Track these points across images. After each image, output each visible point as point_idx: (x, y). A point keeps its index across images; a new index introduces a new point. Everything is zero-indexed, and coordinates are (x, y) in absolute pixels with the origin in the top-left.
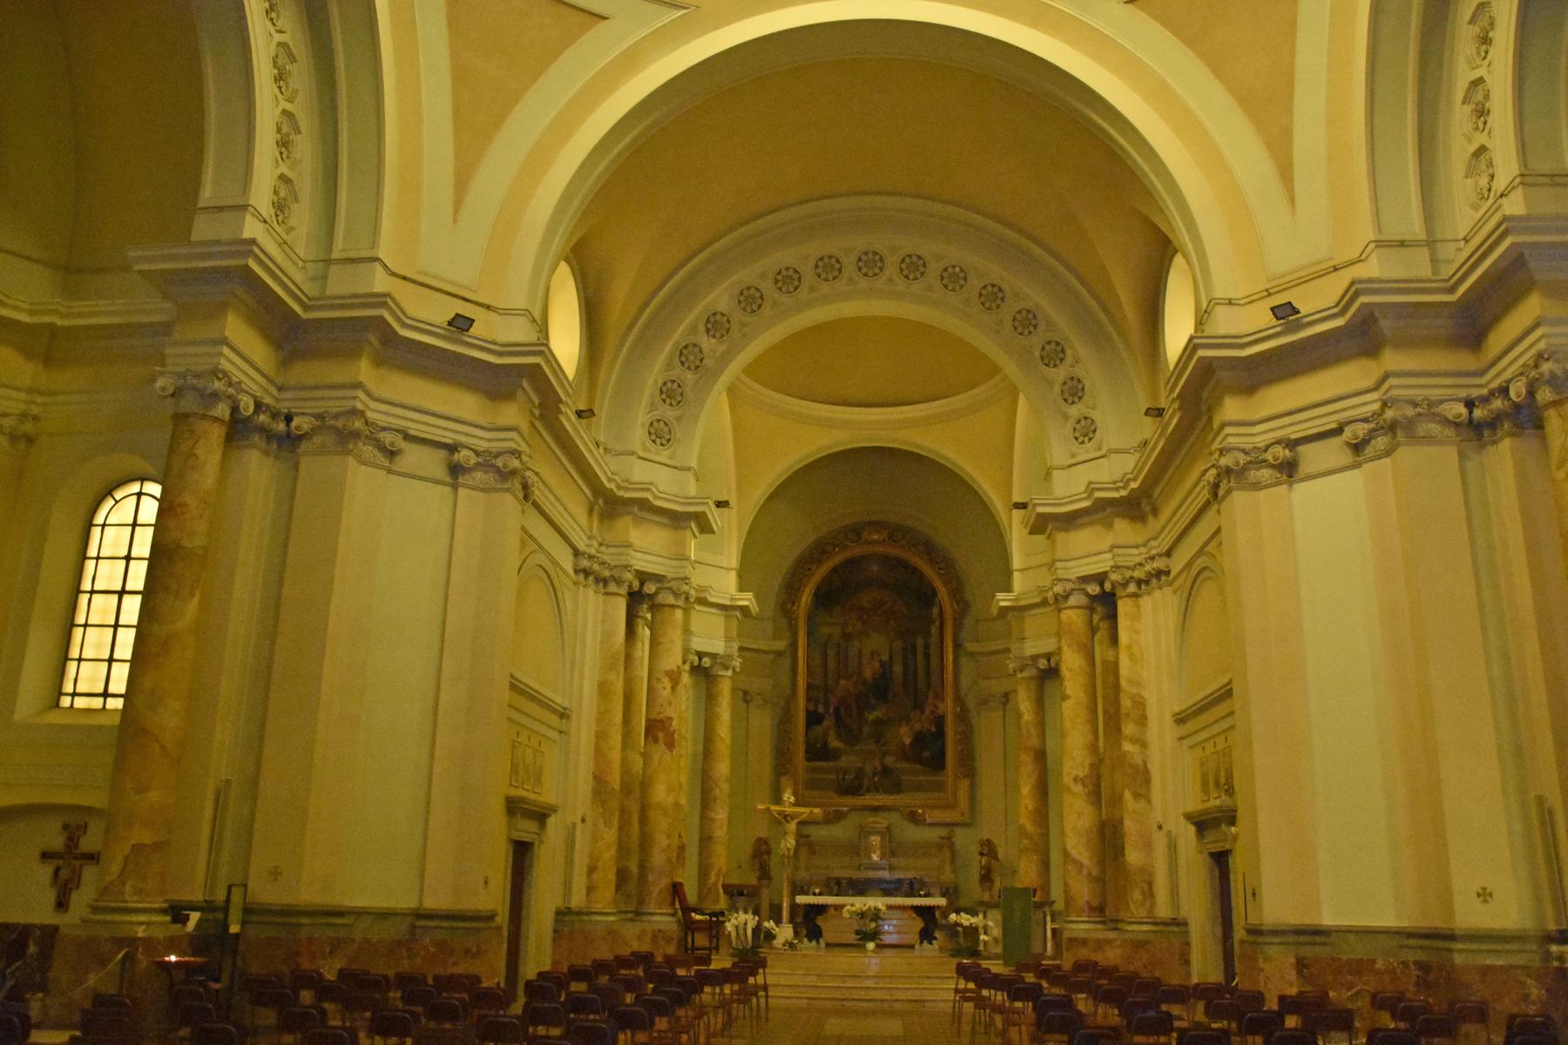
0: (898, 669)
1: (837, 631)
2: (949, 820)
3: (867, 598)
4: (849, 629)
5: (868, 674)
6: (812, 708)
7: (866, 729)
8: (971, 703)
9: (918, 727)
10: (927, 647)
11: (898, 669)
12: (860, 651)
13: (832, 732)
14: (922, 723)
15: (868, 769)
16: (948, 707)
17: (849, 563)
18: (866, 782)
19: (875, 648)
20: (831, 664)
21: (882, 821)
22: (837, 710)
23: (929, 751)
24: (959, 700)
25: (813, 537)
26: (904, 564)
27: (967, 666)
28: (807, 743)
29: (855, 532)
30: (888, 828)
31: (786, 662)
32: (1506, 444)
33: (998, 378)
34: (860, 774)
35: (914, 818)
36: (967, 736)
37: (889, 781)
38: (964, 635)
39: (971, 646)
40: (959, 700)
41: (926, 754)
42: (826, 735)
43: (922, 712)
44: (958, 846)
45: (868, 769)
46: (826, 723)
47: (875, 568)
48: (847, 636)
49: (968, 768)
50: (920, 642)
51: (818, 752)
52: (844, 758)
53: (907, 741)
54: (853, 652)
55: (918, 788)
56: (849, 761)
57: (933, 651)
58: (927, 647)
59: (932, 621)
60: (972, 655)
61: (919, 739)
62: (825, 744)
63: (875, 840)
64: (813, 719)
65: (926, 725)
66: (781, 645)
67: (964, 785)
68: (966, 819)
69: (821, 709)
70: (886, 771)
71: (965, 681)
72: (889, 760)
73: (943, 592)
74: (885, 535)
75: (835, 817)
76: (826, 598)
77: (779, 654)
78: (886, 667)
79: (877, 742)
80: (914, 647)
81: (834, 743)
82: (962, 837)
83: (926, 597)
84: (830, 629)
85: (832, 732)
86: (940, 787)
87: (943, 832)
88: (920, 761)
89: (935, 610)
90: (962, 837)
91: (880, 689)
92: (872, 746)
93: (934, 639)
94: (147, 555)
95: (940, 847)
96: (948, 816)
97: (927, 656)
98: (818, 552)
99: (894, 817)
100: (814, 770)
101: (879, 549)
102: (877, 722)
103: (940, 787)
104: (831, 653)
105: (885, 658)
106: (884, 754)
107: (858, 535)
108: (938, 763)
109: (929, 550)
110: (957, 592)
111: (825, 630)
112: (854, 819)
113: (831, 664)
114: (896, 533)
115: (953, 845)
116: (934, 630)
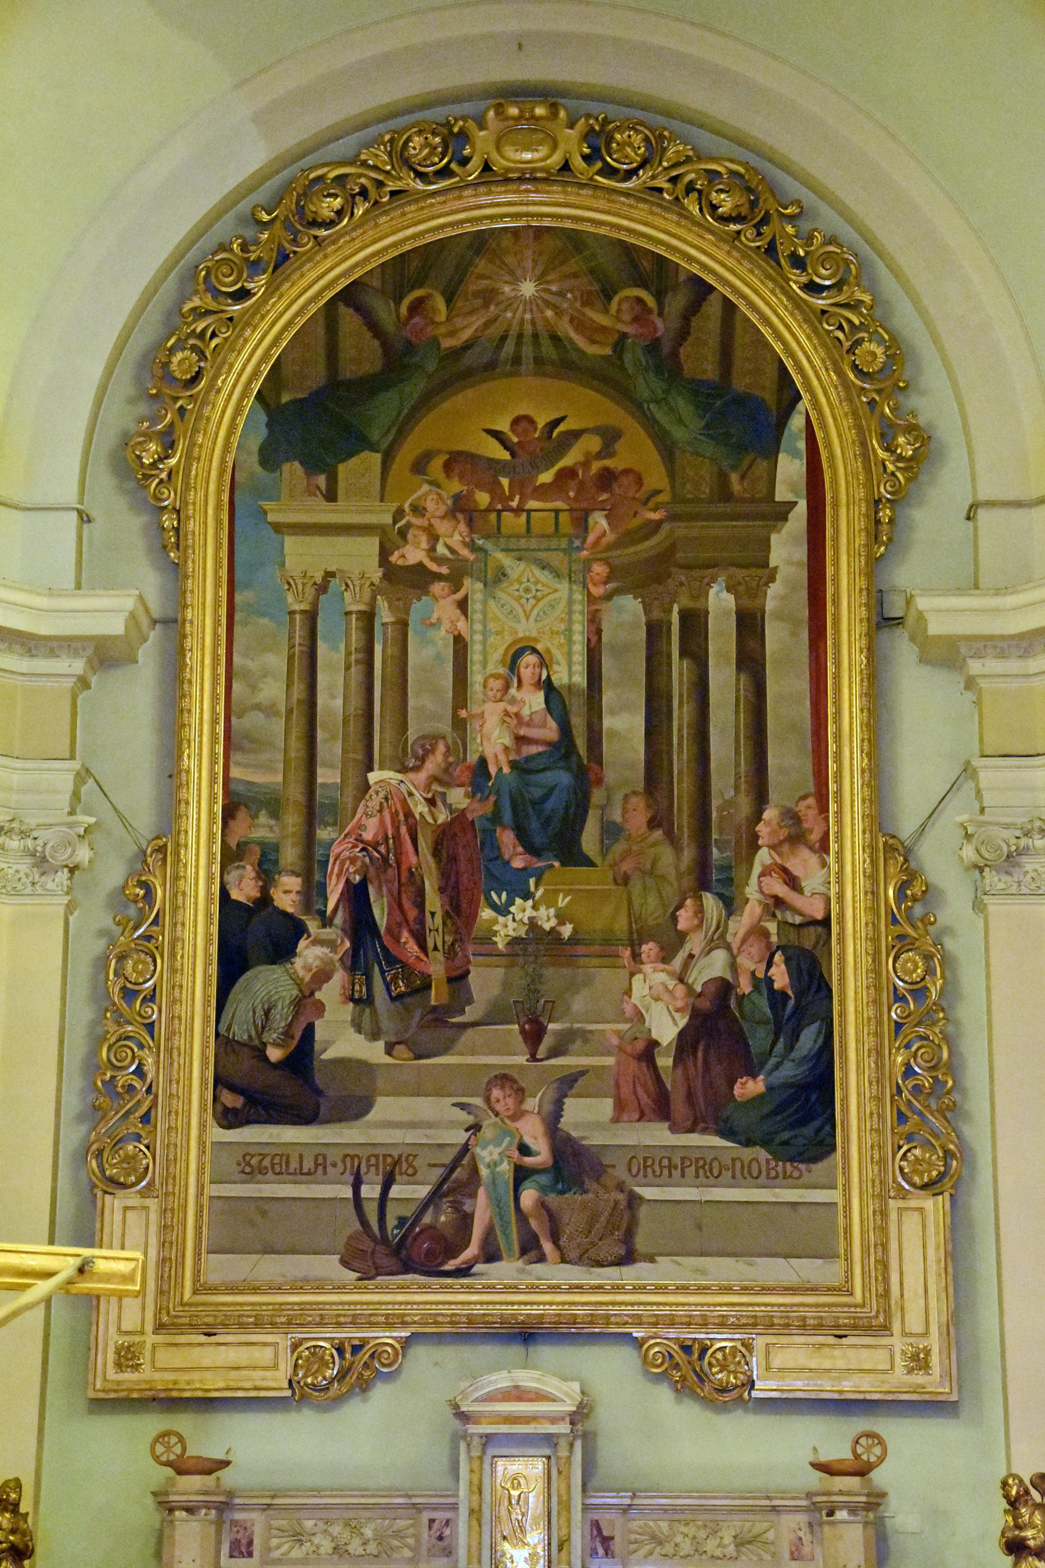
0: (624, 724)
1: (360, 557)
2: (849, 1387)
3: (481, 420)
4: (413, 554)
5: (492, 741)
6: (244, 891)
7: (486, 983)
8: (941, 861)
9: (714, 966)
10: (749, 624)
11: (624, 724)
12: (460, 645)
13: (331, 993)
14: (731, 949)
15: (493, 1157)
16: (844, 883)
17: (406, 271)
18: (481, 1210)
19: (525, 628)
20: (334, 697)
21: (553, 1379)
22: (357, 897)
23: (765, 1074)
24: (892, 850)
25: (253, 156)
26: (655, 272)
27: (922, 699)
28: (224, 1043)
29: (442, 141)
30: (580, 1415)
31: (137, 690)
32: (598, 927)
33: (522, 732)
34: (457, 1179)
35: (695, 1373)
36: (922, 1011)
37: (580, 1204)
38: (906, 575)
39: (943, 613)
40: (892, 850)
41: (750, 1088)
42: (306, 1001)
43: (730, 905)
44: (903, 1516)
45: (493, 1157)
46: (309, 954)
47: (528, 289)
48: (407, 581)
49: (931, 1104)
50: (720, 601)
51: (273, 1084)
52: (384, 1107)
53: (666, 1027)
54: (428, 653)
55: (706, 1235)
56: (413, 1118)
57: (783, 639)
58: (749, 624)
59: (782, 513)
60: (948, 655)
61: (715, 1024)
62: (302, 1055)
63: (523, 1474)
64: (250, 938)
65: (750, 963)
66: (106, 613)
67: (918, 1231)
68: (933, 1382)
69: (287, 894)
70: (572, 1164)
71: (918, 782)
72: (588, 1116)
73: (823, 395)
74: (571, 143)
75: (349, 1372)
76: (317, 420)
77: (105, 656)
78: (573, 711)
79: (534, 1036)
80: (694, 624)
81: (342, 1039)
82: (915, 1461)
83: (751, 414)
84: (330, 546)
85: (331, 993)
86: (812, 1236)
87: (834, 1439)
88: (713, 1114)
89: (790, 469)
90: (915, 1461)
91: (546, 809)
92: (504, 1051)
93: (782, 596)
94: (812, 790)
95: (821, 1510)
96: (861, 1366)
97: (751, 661)
98: (284, 218)
99: (610, 1375)
100: (253, 1166)
101: (549, 207)
102: (537, 943)
103: (812, 1236)
104: (332, 656)
105: (569, 673)
106: (568, 1084)
107: (454, 140)
108: (802, 1122)
109: (760, 208)
110: (883, 383)
111: (305, 557)
112: (432, 1377)
113: (334, 697)
114: (618, 138)
115: (875, 1502)
116: (786, 549)
